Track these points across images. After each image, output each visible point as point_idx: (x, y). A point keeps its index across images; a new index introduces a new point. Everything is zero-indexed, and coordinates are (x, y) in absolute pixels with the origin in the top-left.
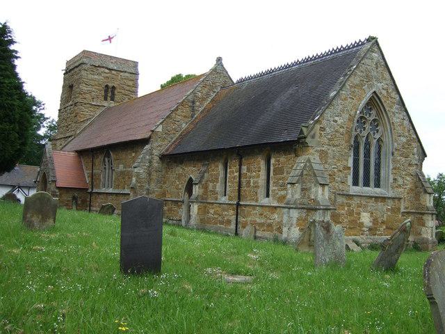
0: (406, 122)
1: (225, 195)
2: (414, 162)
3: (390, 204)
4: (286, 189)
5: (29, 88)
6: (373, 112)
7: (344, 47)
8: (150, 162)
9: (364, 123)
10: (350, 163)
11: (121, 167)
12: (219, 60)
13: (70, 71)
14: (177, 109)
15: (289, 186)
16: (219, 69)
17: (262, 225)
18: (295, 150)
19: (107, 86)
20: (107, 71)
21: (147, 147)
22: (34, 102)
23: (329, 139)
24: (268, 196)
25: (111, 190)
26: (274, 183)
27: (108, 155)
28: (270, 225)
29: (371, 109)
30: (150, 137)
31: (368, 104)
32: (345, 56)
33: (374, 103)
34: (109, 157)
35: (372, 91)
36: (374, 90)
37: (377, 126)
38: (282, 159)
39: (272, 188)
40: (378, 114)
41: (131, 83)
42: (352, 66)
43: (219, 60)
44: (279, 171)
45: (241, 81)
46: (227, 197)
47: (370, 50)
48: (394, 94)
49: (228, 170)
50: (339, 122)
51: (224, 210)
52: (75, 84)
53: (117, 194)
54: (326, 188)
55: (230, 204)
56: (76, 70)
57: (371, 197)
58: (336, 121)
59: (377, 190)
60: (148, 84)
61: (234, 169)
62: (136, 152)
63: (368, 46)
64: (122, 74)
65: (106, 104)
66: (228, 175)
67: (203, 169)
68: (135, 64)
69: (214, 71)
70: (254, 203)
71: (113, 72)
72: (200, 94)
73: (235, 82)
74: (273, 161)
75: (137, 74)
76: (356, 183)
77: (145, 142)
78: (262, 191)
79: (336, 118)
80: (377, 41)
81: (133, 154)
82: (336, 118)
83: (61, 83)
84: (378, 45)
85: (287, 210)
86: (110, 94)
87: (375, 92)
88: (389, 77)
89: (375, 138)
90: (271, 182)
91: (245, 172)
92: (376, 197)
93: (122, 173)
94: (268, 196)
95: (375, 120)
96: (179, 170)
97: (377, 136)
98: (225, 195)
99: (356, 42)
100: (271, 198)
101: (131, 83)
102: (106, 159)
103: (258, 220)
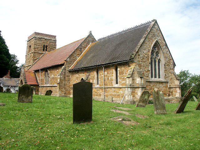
0: (168, 53)
1: (98, 84)
2: (172, 68)
3: (164, 84)
4: (126, 80)
5: (11, 52)
6: (156, 49)
7: (143, 24)
8: (65, 73)
9: (153, 53)
10: (150, 69)
11: (53, 76)
12: (91, 32)
13: (30, 40)
14: (74, 52)
15: (127, 79)
16: (90, 35)
17: (115, 95)
18: (128, 64)
19: (44, 45)
20: (44, 40)
21: (63, 67)
22: (14, 57)
23: (142, 59)
24: (117, 83)
25: (48, 85)
26: (120, 78)
27: (47, 71)
28: (119, 95)
29: (155, 48)
30: (64, 63)
31: (154, 45)
32: (144, 27)
33: (157, 45)
34: (47, 72)
35: (156, 40)
36: (156, 40)
37: (158, 54)
38: (123, 68)
39: (119, 80)
40: (158, 49)
41: (53, 44)
42: (148, 30)
43: (91, 32)
44: (122, 73)
45: (100, 39)
46: (99, 85)
47: (154, 25)
48: (163, 42)
49: (99, 74)
50: (145, 53)
51: (97, 90)
52: (31, 45)
53: (51, 86)
54: (142, 79)
55: (100, 88)
56: (32, 40)
57: (158, 82)
58: (144, 52)
59: (159, 79)
60: (59, 45)
61: (101, 73)
62: (58, 69)
63: (153, 23)
64: (50, 41)
65: (44, 52)
66: (99, 76)
67: (87, 74)
68: (55, 37)
69: (89, 36)
70: (111, 87)
71: (47, 40)
72: (83, 45)
73: (97, 40)
74: (118, 69)
75: (55, 41)
76: (152, 77)
77: (62, 65)
78: (114, 82)
79: (144, 51)
80: (156, 21)
81: (57, 70)
82: (144, 51)
83: (27, 45)
84: (157, 23)
85: (127, 88)
86: (45, 49)
87: (157, 41)
88: (161, 35)
89: (158, 59)
90: (118, 78)
91: (106, 74)
92: (159, 82)
93: (53, 78)
94: (117, 83)
95: (157, 52)
96: (77, 75)
97: (158, 58)
98: (98, 84)
99: (148, 22)
100: (118, 84)
101: (53, 44)
102: (46, 73)
103: (113, 94)
